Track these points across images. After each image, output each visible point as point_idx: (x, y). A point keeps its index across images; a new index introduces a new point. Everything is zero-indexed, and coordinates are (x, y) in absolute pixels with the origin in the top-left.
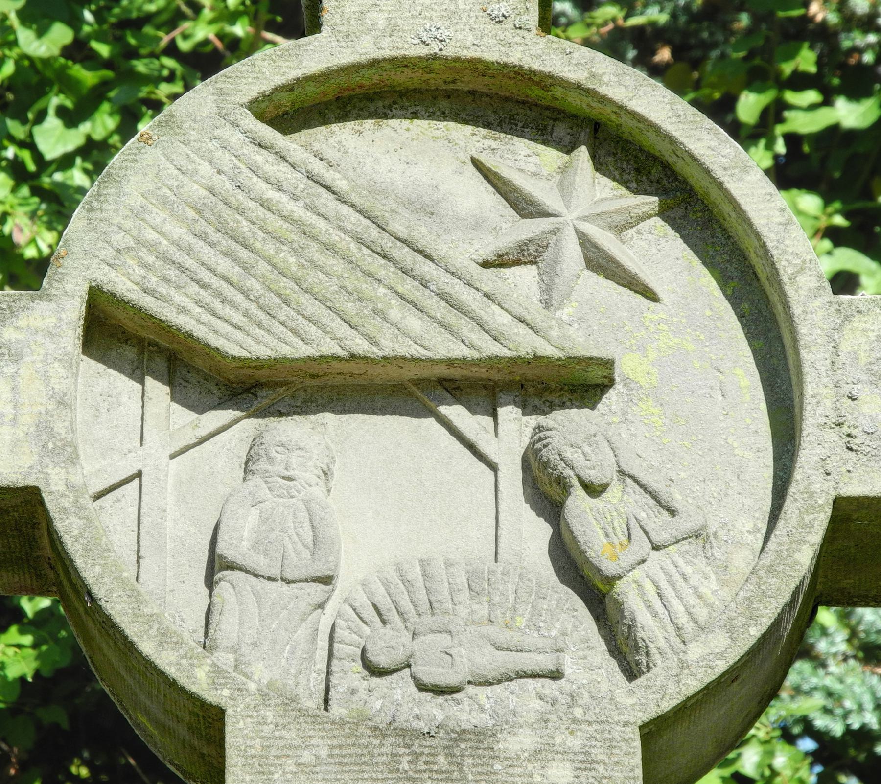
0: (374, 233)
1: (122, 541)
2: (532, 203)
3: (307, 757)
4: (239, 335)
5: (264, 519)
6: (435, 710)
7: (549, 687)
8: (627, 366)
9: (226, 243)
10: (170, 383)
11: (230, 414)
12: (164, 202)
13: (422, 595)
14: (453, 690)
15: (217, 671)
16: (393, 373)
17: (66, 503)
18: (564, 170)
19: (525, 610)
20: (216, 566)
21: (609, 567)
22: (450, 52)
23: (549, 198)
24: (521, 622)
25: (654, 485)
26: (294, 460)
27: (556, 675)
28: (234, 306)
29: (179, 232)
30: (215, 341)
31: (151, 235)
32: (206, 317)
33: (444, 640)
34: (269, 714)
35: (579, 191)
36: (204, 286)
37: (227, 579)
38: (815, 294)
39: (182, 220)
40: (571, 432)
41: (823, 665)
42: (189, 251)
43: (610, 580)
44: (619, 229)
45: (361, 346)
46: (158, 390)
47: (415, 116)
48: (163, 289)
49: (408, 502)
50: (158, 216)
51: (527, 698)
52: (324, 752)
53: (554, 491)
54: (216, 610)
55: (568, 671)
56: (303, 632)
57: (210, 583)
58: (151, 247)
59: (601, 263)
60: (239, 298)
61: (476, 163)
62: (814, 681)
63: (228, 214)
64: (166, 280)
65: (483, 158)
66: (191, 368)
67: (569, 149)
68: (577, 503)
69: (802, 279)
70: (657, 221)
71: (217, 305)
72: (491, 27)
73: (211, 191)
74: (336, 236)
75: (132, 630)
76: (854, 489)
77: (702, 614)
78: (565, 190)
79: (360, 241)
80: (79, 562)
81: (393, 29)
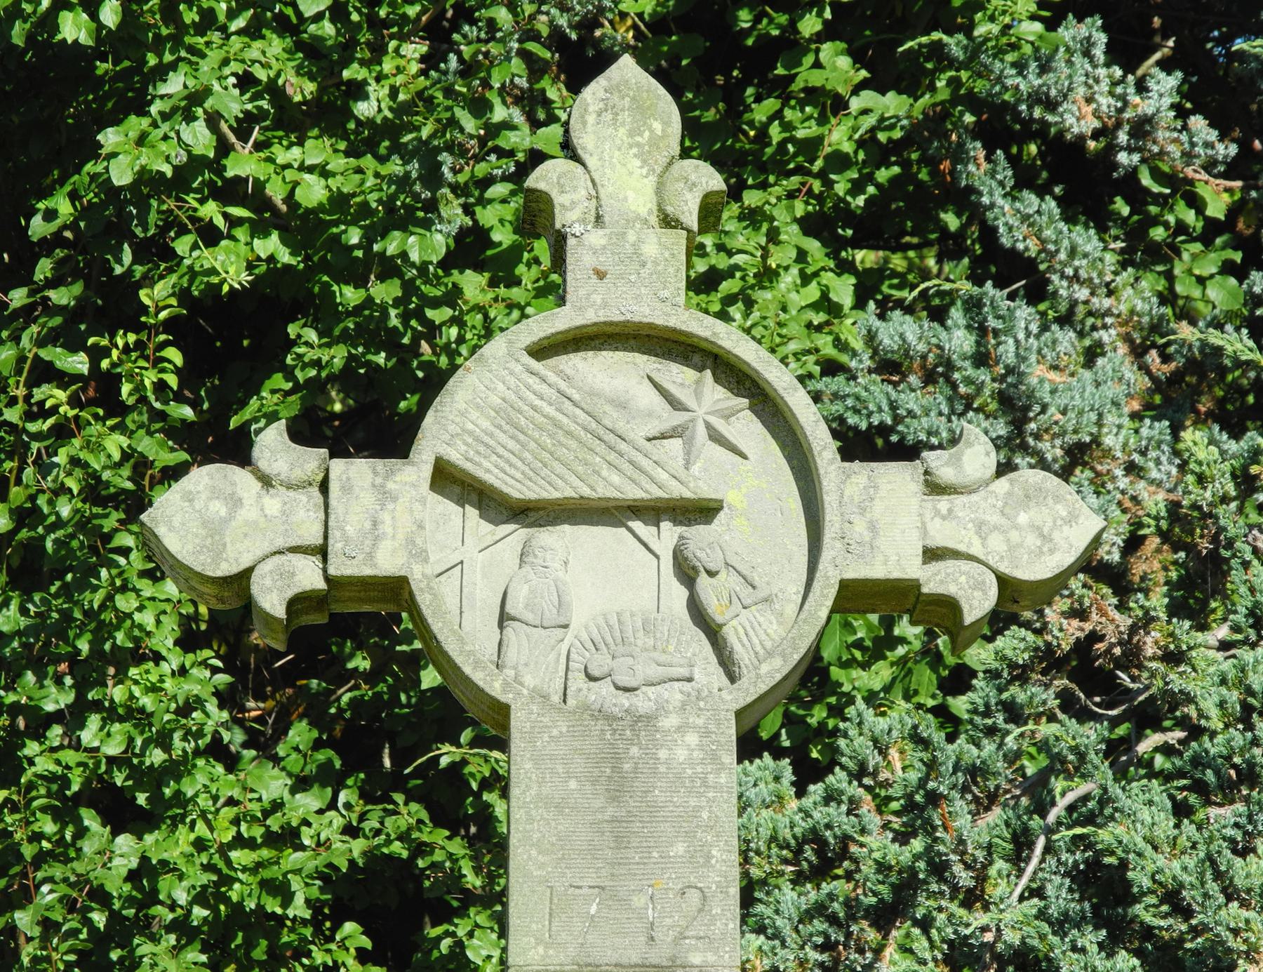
0: (594, 425)
1: (452, 602)
2: (680, 403)
3: (555, 732)
4: (518, 485)
5: (531, 591)
6: (625, 700)
7: (687, 686)
8: (731, 497)
9: (512, 431)
10: (479, 508)
11: (511, 527)
12: (478, 407)
13: (618, 634)
14: (635, 689)
15: (506, 684)
16: (604, 504)
17: (422, 585)
18: (698, 382)
19: (674, 641)
20: (504, 618)
21: (719, 619)
22: (637, 319)
23: (690, 401)
24: (671, 648)
25: (744, 572)
26: (548, 557)
27: (690, 680)
28: (517, 468)
29: (486, 424)
30: (506, 490)
31: (470, 426)
32: (501, 475)
33: (630, 661)
34: (535, 708)
35: (709, 396)
36: (500, 456)
37: (511, 627)
38: (831, 462)
39: (488, 417)
40: (699, 537)
41: (854, 378)
42: (491, 435)
43: (721, 626)
44: (727, 418)
45: (586, 492)
46: (472, 512)
47: (617, 349)
48: (477, 459)
49: (608, 577)
50: (474, 415)
51: (674, 694)
52: (564, 730)
53: (691, 573)
54: (505, 643)
55: (696, 677)
56: (552, 657)
57: (501, 626)
58: (471, 433)
59: (716, 437)
60: (519, 464)
61: (649, 378)
62: (847, 390)
63: (512, 413)
64: (478, 453)
65: (653, 375)
66: (491, 499)
67: (700, 369)
68: (703, 581)
69: (825, 454)
70: (748, 412)
71: (507, 468)
72: (659, 305)
73: (504, 400)
74: (573, 427)
75: (459, 660)
76: (850, 575)
77: (769, 644)
78: (698, 395)
79: (585, 429)
80: (430, 620)
81: (605, 305)
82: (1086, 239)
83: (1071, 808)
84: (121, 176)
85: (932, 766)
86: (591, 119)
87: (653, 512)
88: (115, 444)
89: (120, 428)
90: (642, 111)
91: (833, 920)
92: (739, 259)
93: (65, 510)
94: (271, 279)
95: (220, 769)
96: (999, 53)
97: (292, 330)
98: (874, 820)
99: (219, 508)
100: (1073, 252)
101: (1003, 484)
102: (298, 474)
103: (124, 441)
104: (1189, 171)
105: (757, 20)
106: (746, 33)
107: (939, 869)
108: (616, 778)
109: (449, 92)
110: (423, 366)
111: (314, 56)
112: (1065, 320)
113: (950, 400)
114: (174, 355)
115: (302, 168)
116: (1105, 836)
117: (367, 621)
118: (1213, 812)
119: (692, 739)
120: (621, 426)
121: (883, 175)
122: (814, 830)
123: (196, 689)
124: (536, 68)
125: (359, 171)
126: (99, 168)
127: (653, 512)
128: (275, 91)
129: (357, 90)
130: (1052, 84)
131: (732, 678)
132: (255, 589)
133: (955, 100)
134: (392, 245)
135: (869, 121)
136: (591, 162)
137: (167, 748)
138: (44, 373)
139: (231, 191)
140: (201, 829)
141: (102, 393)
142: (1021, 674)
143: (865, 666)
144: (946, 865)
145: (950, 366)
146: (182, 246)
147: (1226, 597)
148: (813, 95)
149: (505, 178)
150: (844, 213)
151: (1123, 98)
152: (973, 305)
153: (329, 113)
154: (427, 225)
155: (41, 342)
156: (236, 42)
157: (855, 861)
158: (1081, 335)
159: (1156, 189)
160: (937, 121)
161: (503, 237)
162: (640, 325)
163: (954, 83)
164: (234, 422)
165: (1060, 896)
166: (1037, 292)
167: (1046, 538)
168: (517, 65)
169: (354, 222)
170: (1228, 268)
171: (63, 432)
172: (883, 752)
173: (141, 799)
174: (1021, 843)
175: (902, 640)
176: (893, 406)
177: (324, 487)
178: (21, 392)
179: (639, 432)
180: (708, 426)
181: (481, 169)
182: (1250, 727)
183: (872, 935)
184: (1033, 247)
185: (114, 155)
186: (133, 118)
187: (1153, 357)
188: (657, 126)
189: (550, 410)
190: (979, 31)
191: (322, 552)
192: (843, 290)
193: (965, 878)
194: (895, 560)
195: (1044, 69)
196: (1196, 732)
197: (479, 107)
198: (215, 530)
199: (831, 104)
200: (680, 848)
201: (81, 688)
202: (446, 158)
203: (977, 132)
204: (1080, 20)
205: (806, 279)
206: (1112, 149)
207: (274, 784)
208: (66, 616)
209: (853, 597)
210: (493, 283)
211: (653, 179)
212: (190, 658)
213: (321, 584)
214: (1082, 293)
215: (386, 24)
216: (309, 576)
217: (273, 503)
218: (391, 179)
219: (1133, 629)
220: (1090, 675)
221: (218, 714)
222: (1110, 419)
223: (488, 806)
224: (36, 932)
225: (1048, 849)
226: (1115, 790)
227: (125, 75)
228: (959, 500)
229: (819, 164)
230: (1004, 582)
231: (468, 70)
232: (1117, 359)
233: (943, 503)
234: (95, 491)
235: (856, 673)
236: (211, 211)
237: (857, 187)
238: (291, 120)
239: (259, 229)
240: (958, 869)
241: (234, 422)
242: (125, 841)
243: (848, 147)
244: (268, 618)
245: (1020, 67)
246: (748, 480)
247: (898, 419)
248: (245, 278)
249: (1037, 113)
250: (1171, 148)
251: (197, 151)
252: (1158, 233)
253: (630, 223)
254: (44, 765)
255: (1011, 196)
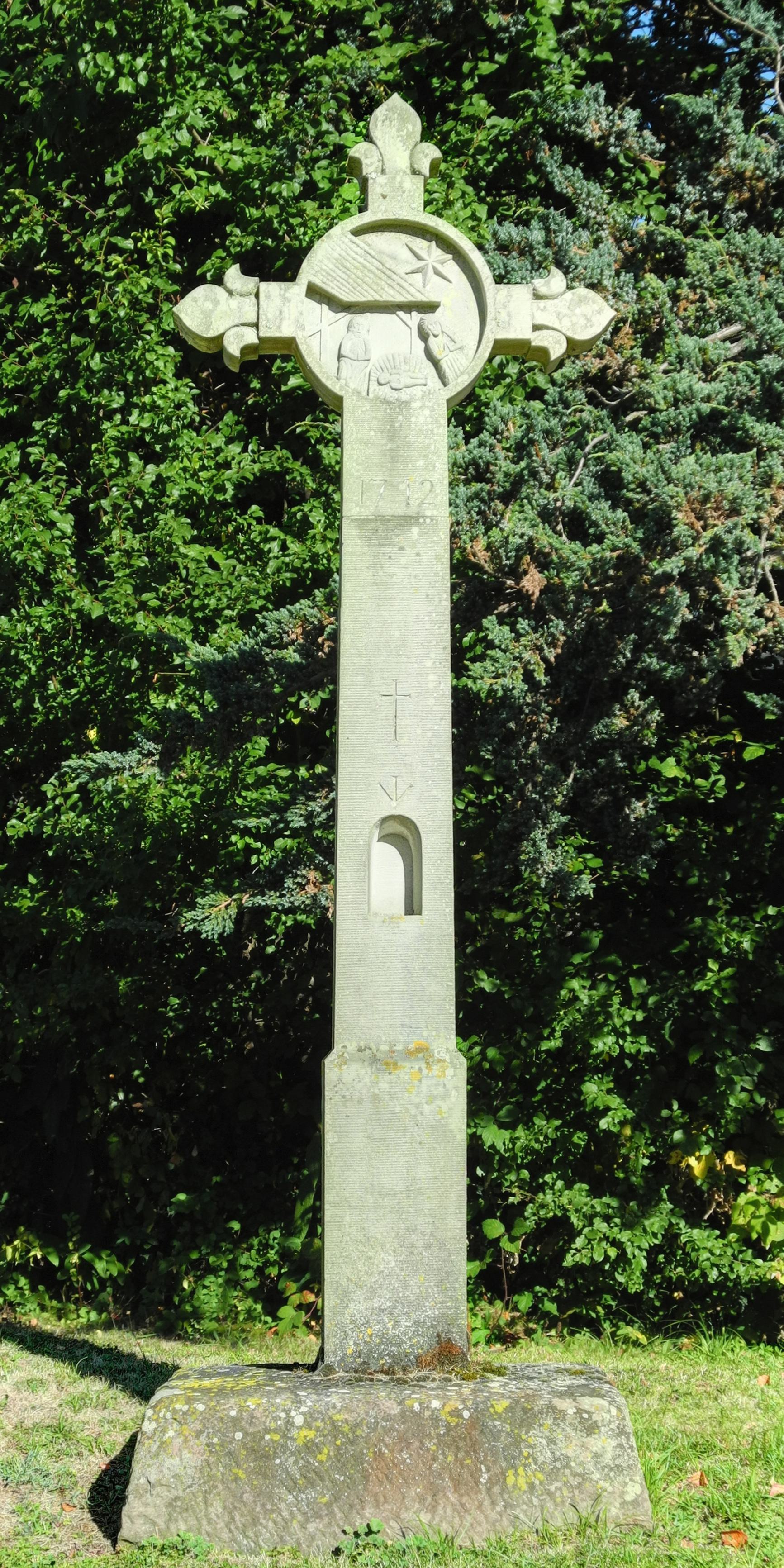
1: (316, 350)
6: (395, 394)
8: (445, 301)
20: (340, 357)
21: (439, 357)
35: (433, 254)
37: (343, 360)
45: (378, 298)
46: (325, 307)
49: (390, 335)
50: (326, 262)
51: (418, 391)
59: (437, 273)
68: (431, 340)
75: (320, 375)
76: (500, 336)
78: (429, 252)
82: (595, 188)
83: (595, 447)
84: (149, 155)
85: (530, 428)
86: (379, 124)
87: (408, 307)
88: (145, 282)
89: (147, 275)
90: (403, 120)
91: (482, 500)
92: (435, 196)
93: (122, 313)
94: (218, 203)
95: (194, 434)
96: (556, 100)
97: (228, 229)
98: (502, 454)
99: (209, 305)
100: (589, 194)
101: (569, 294)
102: (245, 289)
103: (148, 280)
104: (642, 156)
105: (442, 83)
106: (436, 89)
107: (534, 474)
108: (393, 432)
109: (301, 116)
110: (287, 246)
111: (236, 100)
112: (585, 226)
113: (532, 263)
114: (172, 240)
115: (233, 152)
116: (611, 457)
117: (272, 360)
118: (661, 447)
119: (427, 412)
120: (393, 267)
121: (500, 157)
122: (474, 459)
123: (183, 397)
124: (341, 105)
125: (258, 153)
126: (138, 152)
127: (408, 307)
128: (218, 116)
129: (256, 115)
130: (583, 112)
131: (445, 385)
132: (226, 342)
133: (535, 121)
134: (274, 188)
135: (495, 131)
136: (379, 144)
137: (170, 425)
138: (113, 249)
139: (198, 164)
140: (186, 463)
141: (138, 259)
142: (573, 384)
143: (492, 388)
144: (537, 473)
145: (531, 247)
146: (175, 189)
147: (664, 351)
148: (468, 119)
149: (325, 157)
150: (482, 175)
151: (612, 121)
152: (544, 219)
153: (244, 126)
154: (291, 179)
155: (112, 233)
156: (200, 92)
157: (493, 474)
158: (592, 233)
159: (627, 164)
160: (527, 130)
161: (324, 185)
162: (403, 221)
163: (535, 114)
164: (199, 272)
165: (590, 486)
166: (572, 213)
167: (588, 320)
168: (333, 103)
169: (256, 178)
170: (659, 202)
171: (120, 277)
172: (506, 424)
173: (158, 448)
174: (571, 463)
175: (508, 376)
176: (505, 266)
177: (257, 296)
178: (102, 258)
179: (402, 270)
180: (434, 268)
181: (315, 153)
182: (677, 408)
183: (500, 506)
184: (570, 191)
185: (144, 145)
186: (153, 129)
187: (625, 244)
188: (410, 127)
189: (361, 260)
190: (547, 89)
191: (256, 326)
192: (482, 211)
193: (546, 479)
194: (520, 331)
195: (576, 108)
196: (652, 410)
197: (316, 123)
198: (207, 315)
199: (476, 123)
200: (421, 463)
201: (128, 396)
202: (299, 147)
203: (544, 137)
204: (593, 84)
205: (466, 206)
206: (606, 146)
207: (218, 441)
208: (122, 363)
209: (500, 346)
210: (321, 207)
211: (408, 152)
212: (180, 383)
213: (256, 341)
214: (593, 214)
215: (270, 84)
216: (251, 337)
217: (234, 303)
218: (273, 157)
219: (625, 363)
220: (600, 385)
221: (193, 408)
222: (606, 272)
223: (319, 451)
224: (109, 509)
225: (585, 465)
226: (617, 436)
227: (149, 109)
228: (549, 302)
229: (472, 151)
230: (569, 340)
231: (308, 106)
232: (609, 244)
233: (542, 303)
234: (135, 303)
235: (487, 391)
236: (190, 173)
237: (489, 163)
238: (224, 130)
239: (211, 181)
240: (543, 474)
241: (199, 272)
242: (151, 468)
243: (484, 144)
244: (231, 357)
245: (565, 106)
246: (451, 291)
247: (507, 272)
248: (207, 204)
249: (573, 128)
250: (635, 145)
251: (184, 144)
252: (627, 186)
253: (397, 172)
254: (112, 433)
255: (560, 167)
